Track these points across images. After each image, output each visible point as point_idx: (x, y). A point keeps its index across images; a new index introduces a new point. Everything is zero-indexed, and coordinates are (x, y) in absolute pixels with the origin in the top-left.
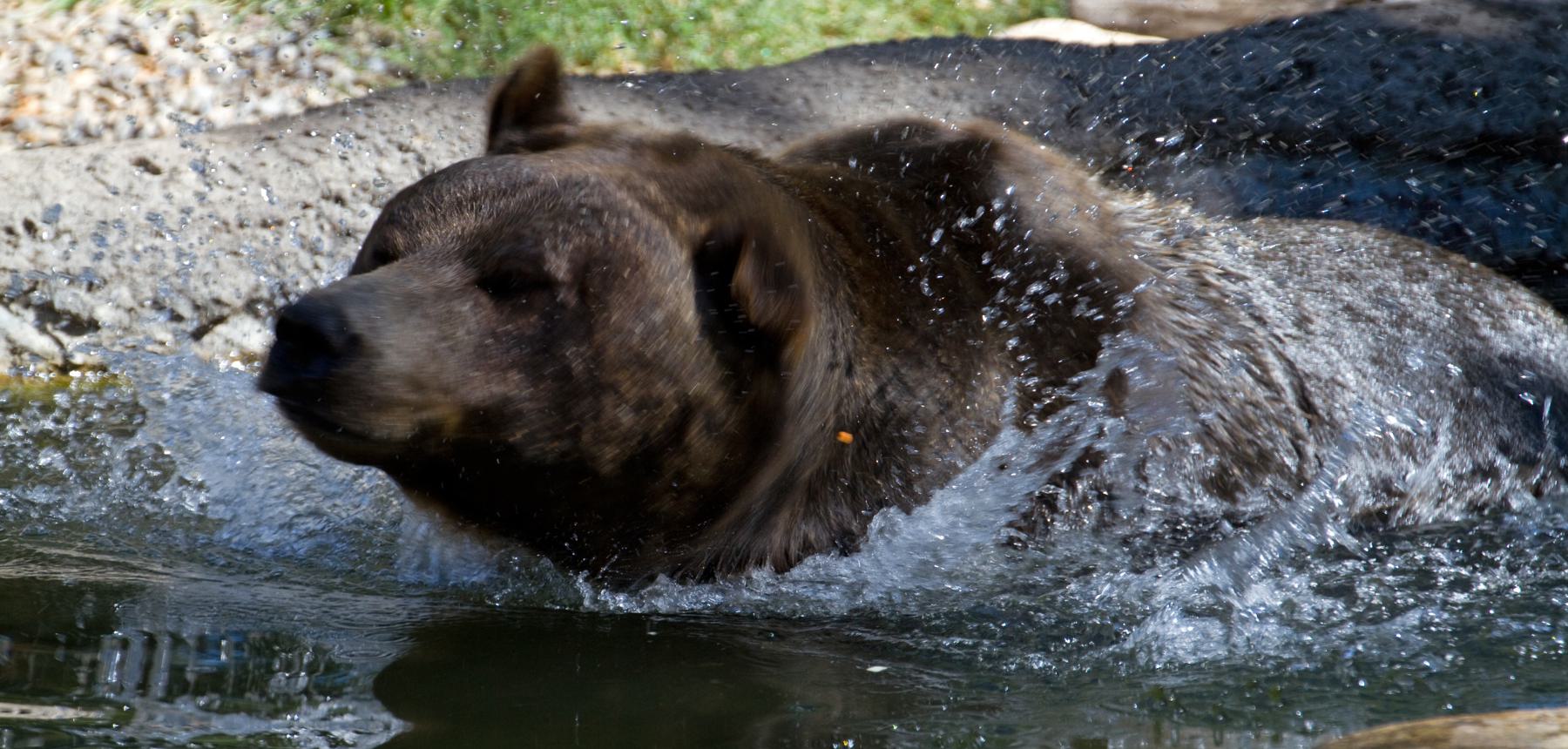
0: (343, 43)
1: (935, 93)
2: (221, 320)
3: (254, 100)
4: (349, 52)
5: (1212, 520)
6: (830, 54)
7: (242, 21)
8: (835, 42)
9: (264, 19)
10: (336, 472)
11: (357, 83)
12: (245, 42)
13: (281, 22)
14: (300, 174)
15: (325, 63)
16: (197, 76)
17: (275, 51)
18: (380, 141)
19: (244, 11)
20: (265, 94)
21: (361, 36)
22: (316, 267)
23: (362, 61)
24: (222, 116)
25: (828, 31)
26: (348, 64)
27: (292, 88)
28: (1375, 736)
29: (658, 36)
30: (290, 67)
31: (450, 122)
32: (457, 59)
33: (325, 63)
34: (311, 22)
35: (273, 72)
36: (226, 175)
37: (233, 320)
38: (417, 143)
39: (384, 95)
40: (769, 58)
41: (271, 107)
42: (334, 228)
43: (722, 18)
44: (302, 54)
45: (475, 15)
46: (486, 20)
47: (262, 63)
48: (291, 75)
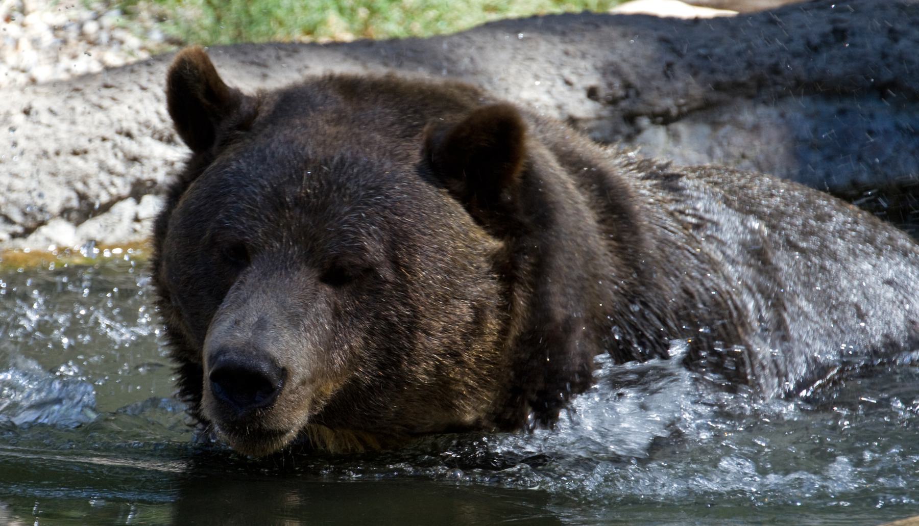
1: (566, 53)
2: (43, 223)
3: (65, 62)
4: (136, 26)
8: (493, 17)
11: (142, 48)
12: (60, 19)
14: (99, 116)
15: (119, 34)
16: (25, 44)
17: (81, 26)
20: (74, 57)
21: (145, 15)
22: (112, 184)
24: (44, 73)
26: (135, 35)
27: (94, 52)
29: (363, 13)
30: (92, 38)
33: (119, 34)
35: (80, 40)
36: (45, 118)
37: (52, 223)
40: (445, 29)
42: (125, 155)
44: (101, 28)
47: (72, 34)
48: (93, 43)
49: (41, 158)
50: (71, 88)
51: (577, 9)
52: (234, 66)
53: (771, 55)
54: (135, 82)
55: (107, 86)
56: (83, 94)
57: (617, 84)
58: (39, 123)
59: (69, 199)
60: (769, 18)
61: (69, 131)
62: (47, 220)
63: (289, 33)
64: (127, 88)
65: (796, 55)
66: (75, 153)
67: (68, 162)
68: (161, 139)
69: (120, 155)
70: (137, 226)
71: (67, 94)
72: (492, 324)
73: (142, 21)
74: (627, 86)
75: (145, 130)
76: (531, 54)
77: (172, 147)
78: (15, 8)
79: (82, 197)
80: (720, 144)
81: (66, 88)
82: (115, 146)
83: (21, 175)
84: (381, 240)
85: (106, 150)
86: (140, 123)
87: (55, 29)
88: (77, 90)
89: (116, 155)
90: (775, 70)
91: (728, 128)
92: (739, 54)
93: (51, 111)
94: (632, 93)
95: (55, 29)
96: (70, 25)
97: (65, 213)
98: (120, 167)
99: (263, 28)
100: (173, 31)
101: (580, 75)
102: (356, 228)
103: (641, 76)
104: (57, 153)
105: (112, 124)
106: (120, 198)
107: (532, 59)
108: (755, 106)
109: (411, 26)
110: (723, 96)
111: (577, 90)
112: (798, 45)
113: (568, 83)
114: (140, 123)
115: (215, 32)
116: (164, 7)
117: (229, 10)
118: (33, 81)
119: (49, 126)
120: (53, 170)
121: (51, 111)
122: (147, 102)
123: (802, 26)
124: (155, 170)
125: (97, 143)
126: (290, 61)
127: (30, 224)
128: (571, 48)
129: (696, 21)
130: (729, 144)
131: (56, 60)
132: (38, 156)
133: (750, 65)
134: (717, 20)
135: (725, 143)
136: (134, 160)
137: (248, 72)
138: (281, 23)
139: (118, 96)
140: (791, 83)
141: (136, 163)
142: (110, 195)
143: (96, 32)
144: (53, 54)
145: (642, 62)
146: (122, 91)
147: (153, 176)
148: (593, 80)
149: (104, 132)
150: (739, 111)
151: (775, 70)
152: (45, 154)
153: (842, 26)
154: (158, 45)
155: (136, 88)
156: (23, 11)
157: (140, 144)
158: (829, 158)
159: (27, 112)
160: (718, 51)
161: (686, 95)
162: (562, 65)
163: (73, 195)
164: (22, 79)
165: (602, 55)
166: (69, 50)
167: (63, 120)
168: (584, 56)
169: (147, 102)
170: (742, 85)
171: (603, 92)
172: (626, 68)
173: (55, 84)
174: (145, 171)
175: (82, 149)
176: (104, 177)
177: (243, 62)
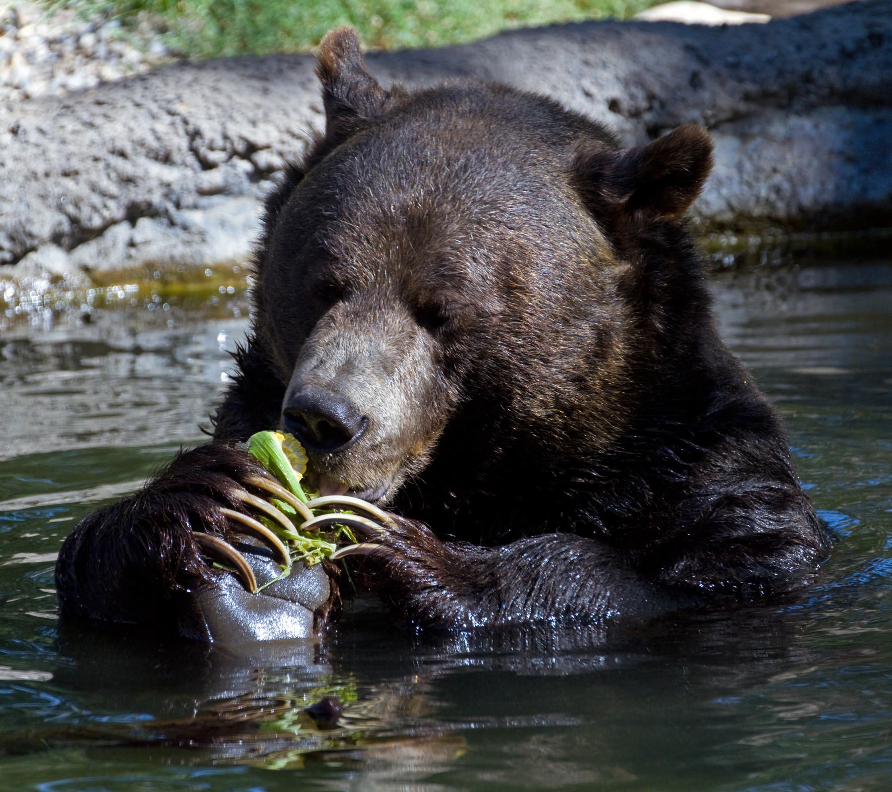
0: (130, 31)
1: (586, 63)
2: (33, 249)
3: (61, 77)
4: (135, 38)
5: (465, 382)
6: (505, 34)
7: (52, 15)
8: (514, 24)
9: (71, 13)
10: (394, 412)
11: (143, 62)
12: (55, 32)
13: (83, 16)
14: (91, 134)
15: (118, 47)
16: (18, 59)
17: (78, 38)
18: (154, 107)
19: (55, 6)
20: (71, 72)
21: (145, 25)
22: (105, 206)
23: (145, 47)
24: (37, 88)
25: (510, 15)
26: (135, 48)
27: (91, 67)
28: (136, 486)
29: (375, 21)
30: (90, 51)
31: (208, 92)
32: (219, 45)
33: (118, 47)
34: (106, 14)
35: (77, 54)
36: (34, 137)
37: (42, 249)
38: (180, 108)
39: (156, 71)
40: (463, 38)
41: (76, 82)
42: (118, 175)
43: (426, 6)
44: (99, 41)
45: (232, 8)
46: (241, 14)
47: (68, 48)
48: (90, 57)
49: (30, 180)
50: (62, 105)
51: (599, 14)
52: (233, 80)
53: (804, 62)
54: (128, 98)
55: (99, 103)
56: (73, 112)
57: (640, 94)
58: (27, 142)
59: (60, 224)
60: (804, 22)
61: (60, 151)
62: (37, 245)
63: (297, 44)
64: (120, 105)
65: (830, 62)
66: (66, 174)
67: (57, 184)
68: (156, 159)
69: (113, 175)
70: (133, 251)
71: (55, 113)
72: (619, 348)
73: (142, 33)
74: (651, 97)
75: (140, 149)
76: (551, 64)
77: (168, 166)
78: (8, 20)
79: (74, 221)
80: (750, 158)
81: (55, 105)
82: (108, 166)
83: (9, 198)
84: (489, 263)
85: (98, 171)
86: (133, 142)
87: (51, 43)
88: (67, 107)
89: (109, 176)
90: (807, 79)
91: (759, 140)
92: (770, 62)
93: (41, 131)
94: (656, 105)
95: (51, 43)
96: (67, 38)
97: (57, 239)
98: (113, 189)
99: (270, 39)
100: (175, 43)
101: (600, 86)
102: (460, 252)
103: (665, 87)
104: (47, 175)
105: (104, 143)
106: (114, 222)
107: (549, 69)
108: (787, 116)
109: (427, 35)
110: (753, 107)
111: (599, 102)
112: (832, 51)
113: (588, 94)
114: (133, 142)
115: (219, 45)
116: (165, 18)
117: (233, 20)
118: (27, 97)
119: (37, 145)
120: (42, 193)
121: (41, 131)
122: (141, 119)
123: (836, 31)
124: (150, 191)
125: (89, 163)
126: (293, 75)
127: (18, 250)
128: (591, 57)
129: (724, 28)
130: (759, 157)
131: (52, 76)
132: (27, 179)
133: (781, 73)
134: (747, 26)
135: (755, 157)
136: (128, 181)
137: (248, 87)
138: (289, 33)
139: (111, 113)
140: (826, 91)
141: (131, 183)
142: (104, 218)
143: (94, 46)
144: (48, 69)
145: (667, 72)
146: (114, 107)
147: (147, 197)
148: (616, 92)
149: (96, 152)
150: (769, 122)
151: (807, 79)
152: (34, 175)
153: (877, 30)
154: (160, 59)
155: (130, 105)
156: (16, 23)
157: (135, 165)
158: (866, 171)
159: (14, 131)
160: (747, 58)
161: (714, 106)
162: (581, 75)
163: (64, 219)
164: (15, 95)
165: (621, 66)
166: (66, 65)
167: (52, 139)
168: (604, 65)
169: (141, 119)
170: (773, 95)
171: (626, 103)
172: (649, 79)
173: (48, 99)
174: (140, 192)
175: (73, 169)
176: (96, 200)
177: (243, 75)
